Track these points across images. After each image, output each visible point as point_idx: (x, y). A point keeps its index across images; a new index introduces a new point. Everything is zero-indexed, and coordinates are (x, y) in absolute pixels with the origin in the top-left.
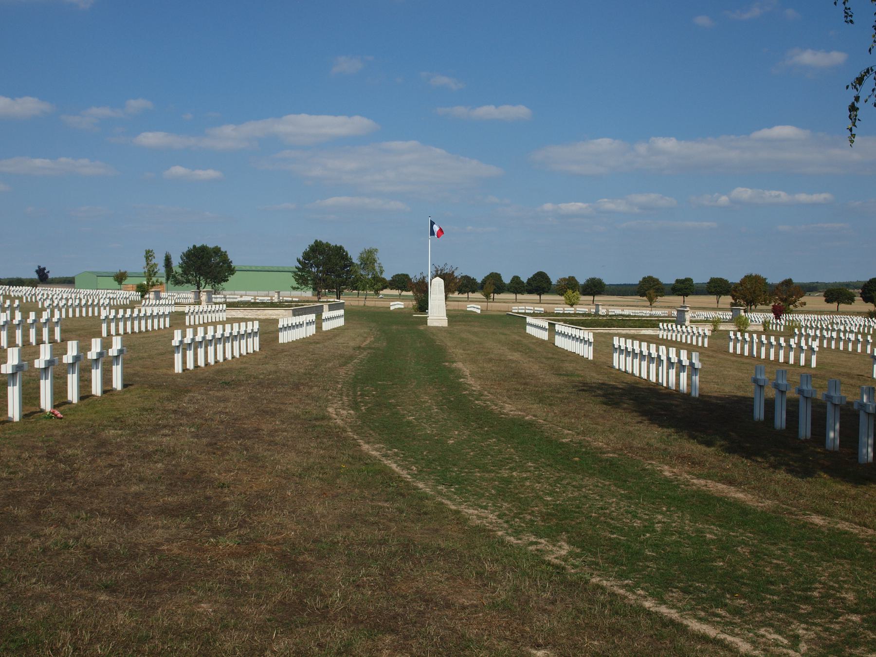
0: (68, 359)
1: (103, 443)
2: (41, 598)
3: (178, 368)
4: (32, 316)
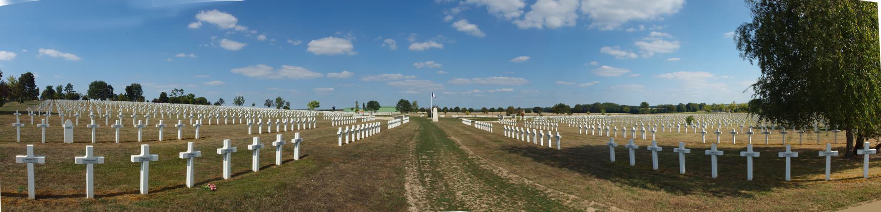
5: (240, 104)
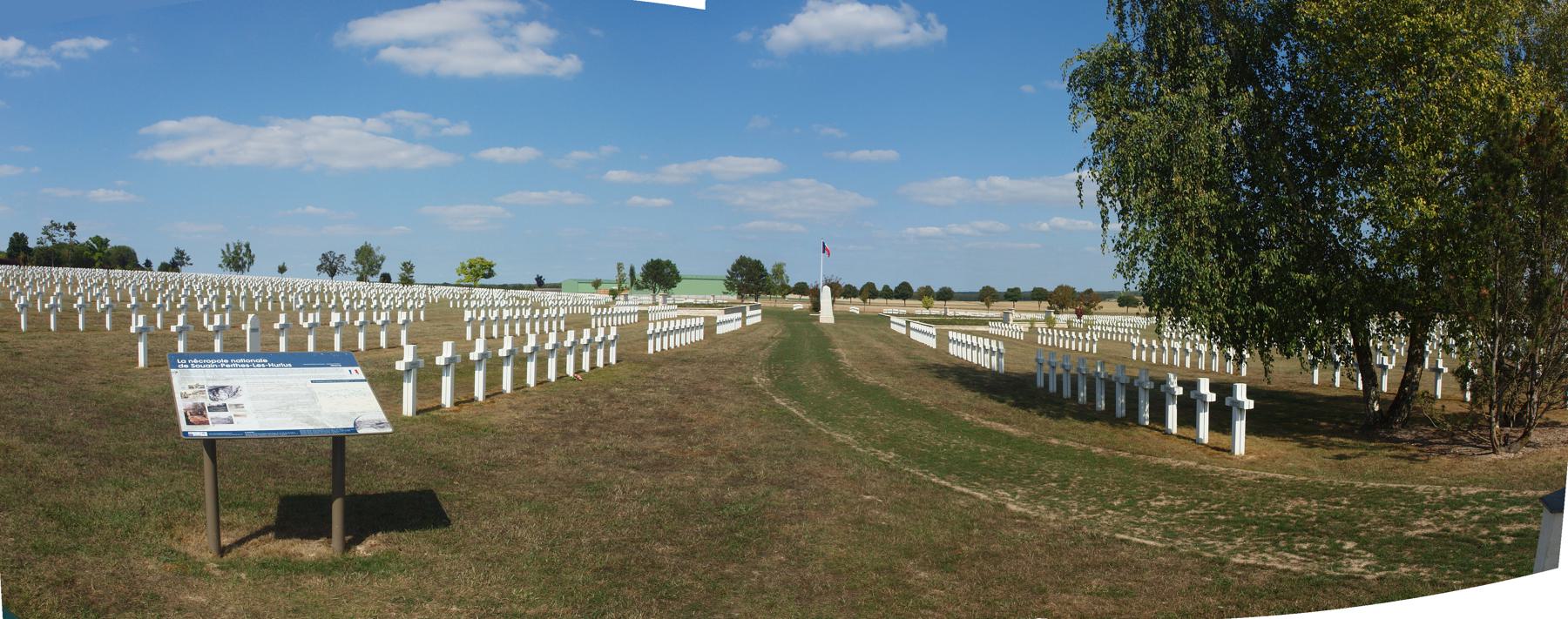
0: (567, 344)
1: (612, 396)
3: (651, 351)
4: (538, 312)
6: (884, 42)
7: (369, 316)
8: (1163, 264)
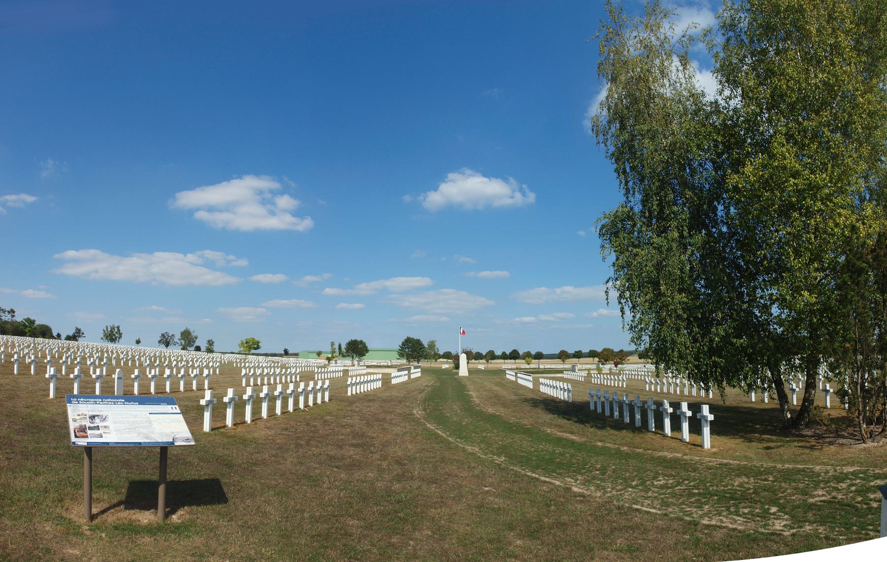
0: (300, 390)
1: (325, 421)
2: (316, 468)
3: (349, 394)
5: (113, 340)
6: (497, 204)
7: (187, 372)
8: (657, 336)
